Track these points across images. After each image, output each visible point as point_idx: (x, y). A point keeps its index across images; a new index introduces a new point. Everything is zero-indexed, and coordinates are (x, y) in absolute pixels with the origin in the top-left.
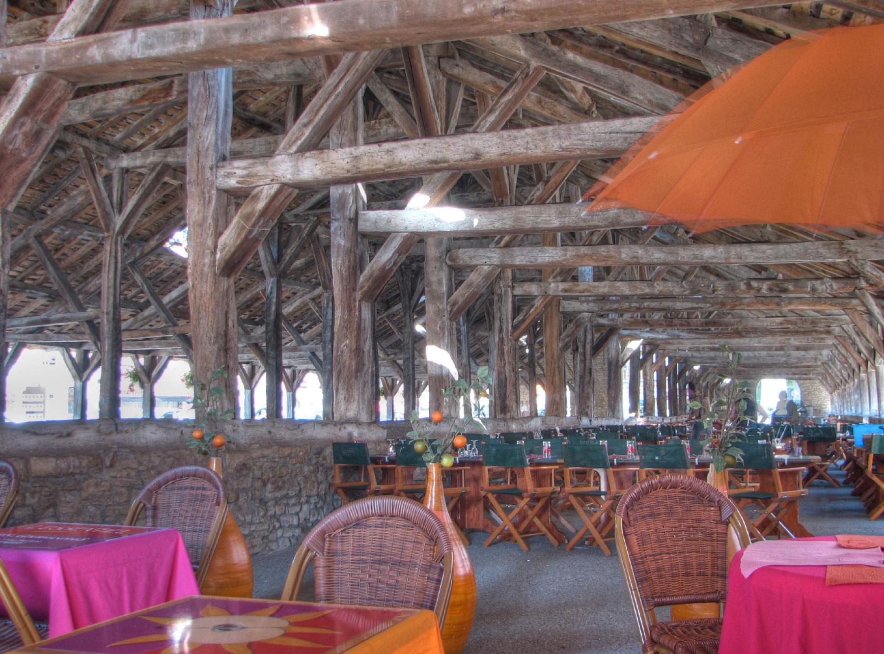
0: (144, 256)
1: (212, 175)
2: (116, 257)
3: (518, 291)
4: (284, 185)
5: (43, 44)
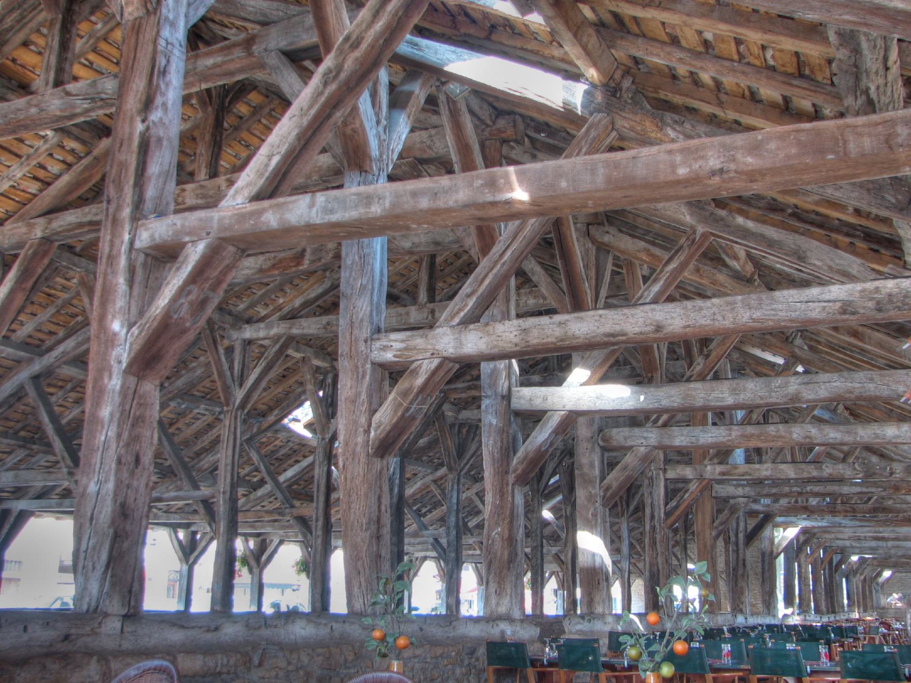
0: (261, 432)
1: (366, 348)
2: (235, 434)
3: (671, 474)
4: (445, 359)
5: (215, 209)
